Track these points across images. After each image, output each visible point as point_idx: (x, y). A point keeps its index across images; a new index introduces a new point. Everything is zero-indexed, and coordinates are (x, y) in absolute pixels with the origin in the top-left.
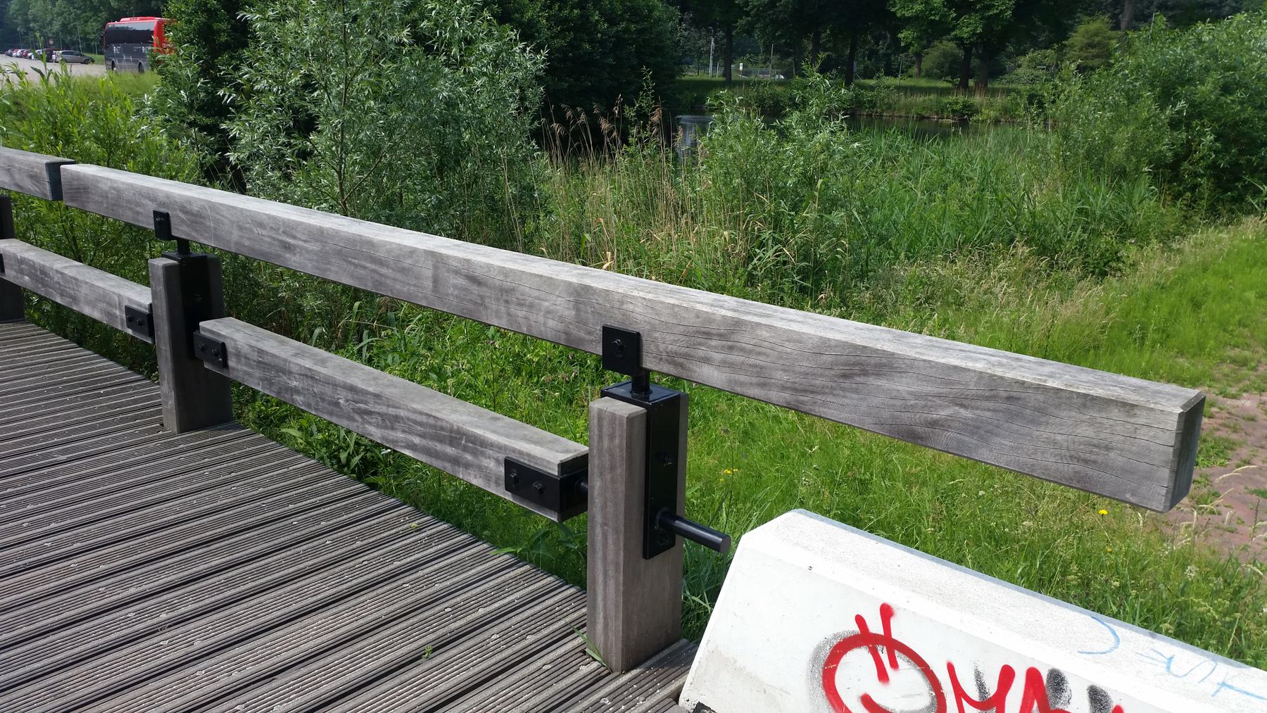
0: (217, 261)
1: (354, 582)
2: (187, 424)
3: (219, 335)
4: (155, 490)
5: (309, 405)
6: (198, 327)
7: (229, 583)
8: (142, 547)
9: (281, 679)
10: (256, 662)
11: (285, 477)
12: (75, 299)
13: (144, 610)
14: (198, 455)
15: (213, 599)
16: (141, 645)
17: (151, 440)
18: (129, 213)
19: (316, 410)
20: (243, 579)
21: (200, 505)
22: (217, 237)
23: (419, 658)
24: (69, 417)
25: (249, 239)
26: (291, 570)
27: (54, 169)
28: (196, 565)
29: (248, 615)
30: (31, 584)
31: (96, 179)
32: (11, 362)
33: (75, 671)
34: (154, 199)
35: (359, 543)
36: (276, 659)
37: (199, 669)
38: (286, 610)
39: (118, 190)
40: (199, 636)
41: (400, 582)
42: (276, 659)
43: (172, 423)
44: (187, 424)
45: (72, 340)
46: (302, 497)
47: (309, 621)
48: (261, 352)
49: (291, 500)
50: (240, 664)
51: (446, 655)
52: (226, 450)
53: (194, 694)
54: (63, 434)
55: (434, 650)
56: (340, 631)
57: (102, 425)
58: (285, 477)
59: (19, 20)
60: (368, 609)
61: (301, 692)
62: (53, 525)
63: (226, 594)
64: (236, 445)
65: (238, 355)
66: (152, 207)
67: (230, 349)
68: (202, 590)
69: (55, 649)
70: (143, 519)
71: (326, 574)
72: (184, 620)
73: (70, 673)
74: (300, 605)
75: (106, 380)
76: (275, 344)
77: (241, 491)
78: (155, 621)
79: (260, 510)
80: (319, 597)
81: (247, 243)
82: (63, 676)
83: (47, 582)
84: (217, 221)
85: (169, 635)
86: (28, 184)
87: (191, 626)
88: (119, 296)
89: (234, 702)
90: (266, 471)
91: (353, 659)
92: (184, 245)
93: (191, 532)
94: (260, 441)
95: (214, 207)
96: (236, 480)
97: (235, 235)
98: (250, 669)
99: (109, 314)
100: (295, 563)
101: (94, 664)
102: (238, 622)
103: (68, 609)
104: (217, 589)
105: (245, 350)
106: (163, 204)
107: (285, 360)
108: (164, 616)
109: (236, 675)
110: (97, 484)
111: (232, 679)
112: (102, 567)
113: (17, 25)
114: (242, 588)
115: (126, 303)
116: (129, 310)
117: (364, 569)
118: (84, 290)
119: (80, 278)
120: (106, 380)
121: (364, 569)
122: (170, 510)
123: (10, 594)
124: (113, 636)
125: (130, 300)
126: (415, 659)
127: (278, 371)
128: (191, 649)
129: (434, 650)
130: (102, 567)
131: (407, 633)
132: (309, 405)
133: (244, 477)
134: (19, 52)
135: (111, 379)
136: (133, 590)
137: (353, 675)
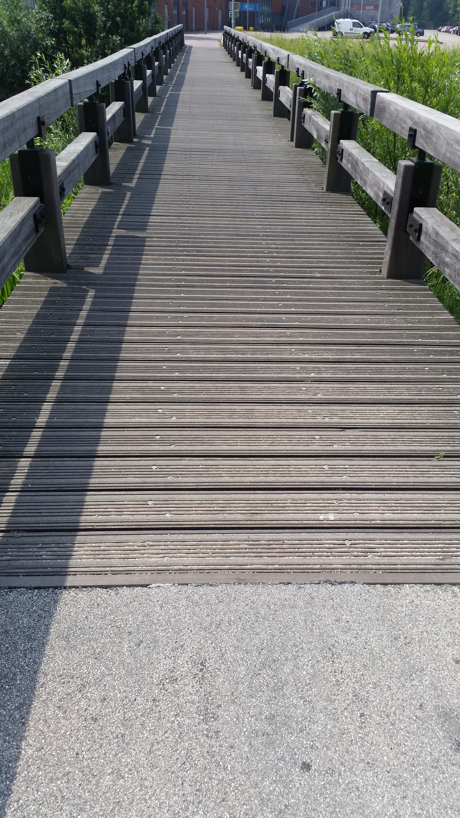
0: (439, 168)
1: (426, 397)
2: (393, 274)
3: (421, 218)
4: (218, 270)
5: (451, 277)
6: (412, 211)
7: (357, 371)
8: (326, 335)
9: (348, 432)
10: (342, 418)
11: (428, 322)
12: (365, 182)
13: (305, 368)
14: (389, 294)
15: (342, 376)
16: (292, 385)
17: (369, 278)
18: (399, 128)
19: (454, 281)
20: (365, 371)
21: (370, 322)
22: (435, 149)
23: (433, 457)
24: (336, 254)
25: (450, 152)
26: (394, 376)
27: (374, 94)
28: (346, 355)
29: (353, 391)
30: (264, 335)
31: (390, 103)
32: (327, 216)
33: (256, 385)
34: (412, 119)
35: (445, 376)
36: (352, 421)
37: (310, 409)
38: (376, 397)
39: (419, 118)
40: (323, 392)
41: (453, 408)
42: (352, 421)
43: (385, 273)
44: (393, 274)
45: (365, 210)
46: (430, 337)
47: (384, 408)
48: (437, 233)
49: (422, 337)
50: (332, 415)
51: (451, 463)
52: (405, 295)
53: (300, 420)
54: (327, 263)
55: (445, 457)
56: (397, 421)
57: (350, 263)
58: (428, 322)
59: (451, 6)
60: (423, 416)
61: (353, 444)
62: (292, 309)
63: (350, 376)
64: (419, 295)
65: (426, 234)
66: (410, 124)
67: (424, 229)
68: (340, 369)
69: (255, 370)
70: (336, 321)
71: (412, 386)
72: (321, 381)
73: (253, 385)
74: (385, 397)
75: (368, 237)
76: (448, 229)
77: (398, 322)
78: (307, 376)
79: (401, 336)
80: (399, 397)
81: (448, 155)
82: (249, 385)
83: (272, 337)
84: (438, 138)
85: (308, 385)
86: (361, 104)
87: (322, 385)
88: (384, 183)
89: (316, 433)
90: (420, 314)
91: (393, 439)
92: (422, 154)
93: (356, 336)
94: (429, 296)
95: (438, 126)
96: (400, 314)
97: (443, 149)
98: (336, 420)
99: (377, 195)
100: (400, 373)
101: (266, 385)
102: (346, 393)
103: (272, 354)
104: (348, 371)
105: (430, 231)
106: (415, 123)
107: (447, 242)
108: (313, 375)
109: (327, 420)
110: (325, 294)
111: (323, 421)
112: (301, 339)
113: (450, 8)
114: (361, 376)
115: (385, 189)
116: (385, 193)
117: (437, 392)
118: (370, 177)
119: (370, 169)
120: (368, 237)
121: (437, 392)
122: (351, 321)
123: (253, 337)
124: (283, 375)
125: (388, 187)
126: (430, 456)
127: (442, 249)
128: (314, 397)
129: (445, 457)
130: (301, 339)
131: (435, 440)
132: (451, 277)
133: (405, 314)
134: (445, 29)
135: (372, 237)
136: (307, 356)
137: (387, 448)
